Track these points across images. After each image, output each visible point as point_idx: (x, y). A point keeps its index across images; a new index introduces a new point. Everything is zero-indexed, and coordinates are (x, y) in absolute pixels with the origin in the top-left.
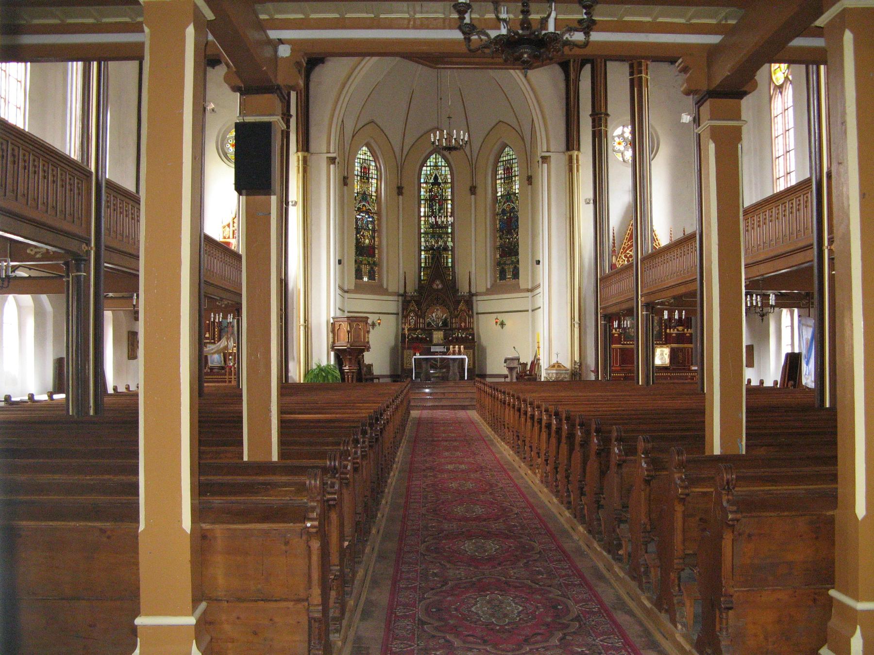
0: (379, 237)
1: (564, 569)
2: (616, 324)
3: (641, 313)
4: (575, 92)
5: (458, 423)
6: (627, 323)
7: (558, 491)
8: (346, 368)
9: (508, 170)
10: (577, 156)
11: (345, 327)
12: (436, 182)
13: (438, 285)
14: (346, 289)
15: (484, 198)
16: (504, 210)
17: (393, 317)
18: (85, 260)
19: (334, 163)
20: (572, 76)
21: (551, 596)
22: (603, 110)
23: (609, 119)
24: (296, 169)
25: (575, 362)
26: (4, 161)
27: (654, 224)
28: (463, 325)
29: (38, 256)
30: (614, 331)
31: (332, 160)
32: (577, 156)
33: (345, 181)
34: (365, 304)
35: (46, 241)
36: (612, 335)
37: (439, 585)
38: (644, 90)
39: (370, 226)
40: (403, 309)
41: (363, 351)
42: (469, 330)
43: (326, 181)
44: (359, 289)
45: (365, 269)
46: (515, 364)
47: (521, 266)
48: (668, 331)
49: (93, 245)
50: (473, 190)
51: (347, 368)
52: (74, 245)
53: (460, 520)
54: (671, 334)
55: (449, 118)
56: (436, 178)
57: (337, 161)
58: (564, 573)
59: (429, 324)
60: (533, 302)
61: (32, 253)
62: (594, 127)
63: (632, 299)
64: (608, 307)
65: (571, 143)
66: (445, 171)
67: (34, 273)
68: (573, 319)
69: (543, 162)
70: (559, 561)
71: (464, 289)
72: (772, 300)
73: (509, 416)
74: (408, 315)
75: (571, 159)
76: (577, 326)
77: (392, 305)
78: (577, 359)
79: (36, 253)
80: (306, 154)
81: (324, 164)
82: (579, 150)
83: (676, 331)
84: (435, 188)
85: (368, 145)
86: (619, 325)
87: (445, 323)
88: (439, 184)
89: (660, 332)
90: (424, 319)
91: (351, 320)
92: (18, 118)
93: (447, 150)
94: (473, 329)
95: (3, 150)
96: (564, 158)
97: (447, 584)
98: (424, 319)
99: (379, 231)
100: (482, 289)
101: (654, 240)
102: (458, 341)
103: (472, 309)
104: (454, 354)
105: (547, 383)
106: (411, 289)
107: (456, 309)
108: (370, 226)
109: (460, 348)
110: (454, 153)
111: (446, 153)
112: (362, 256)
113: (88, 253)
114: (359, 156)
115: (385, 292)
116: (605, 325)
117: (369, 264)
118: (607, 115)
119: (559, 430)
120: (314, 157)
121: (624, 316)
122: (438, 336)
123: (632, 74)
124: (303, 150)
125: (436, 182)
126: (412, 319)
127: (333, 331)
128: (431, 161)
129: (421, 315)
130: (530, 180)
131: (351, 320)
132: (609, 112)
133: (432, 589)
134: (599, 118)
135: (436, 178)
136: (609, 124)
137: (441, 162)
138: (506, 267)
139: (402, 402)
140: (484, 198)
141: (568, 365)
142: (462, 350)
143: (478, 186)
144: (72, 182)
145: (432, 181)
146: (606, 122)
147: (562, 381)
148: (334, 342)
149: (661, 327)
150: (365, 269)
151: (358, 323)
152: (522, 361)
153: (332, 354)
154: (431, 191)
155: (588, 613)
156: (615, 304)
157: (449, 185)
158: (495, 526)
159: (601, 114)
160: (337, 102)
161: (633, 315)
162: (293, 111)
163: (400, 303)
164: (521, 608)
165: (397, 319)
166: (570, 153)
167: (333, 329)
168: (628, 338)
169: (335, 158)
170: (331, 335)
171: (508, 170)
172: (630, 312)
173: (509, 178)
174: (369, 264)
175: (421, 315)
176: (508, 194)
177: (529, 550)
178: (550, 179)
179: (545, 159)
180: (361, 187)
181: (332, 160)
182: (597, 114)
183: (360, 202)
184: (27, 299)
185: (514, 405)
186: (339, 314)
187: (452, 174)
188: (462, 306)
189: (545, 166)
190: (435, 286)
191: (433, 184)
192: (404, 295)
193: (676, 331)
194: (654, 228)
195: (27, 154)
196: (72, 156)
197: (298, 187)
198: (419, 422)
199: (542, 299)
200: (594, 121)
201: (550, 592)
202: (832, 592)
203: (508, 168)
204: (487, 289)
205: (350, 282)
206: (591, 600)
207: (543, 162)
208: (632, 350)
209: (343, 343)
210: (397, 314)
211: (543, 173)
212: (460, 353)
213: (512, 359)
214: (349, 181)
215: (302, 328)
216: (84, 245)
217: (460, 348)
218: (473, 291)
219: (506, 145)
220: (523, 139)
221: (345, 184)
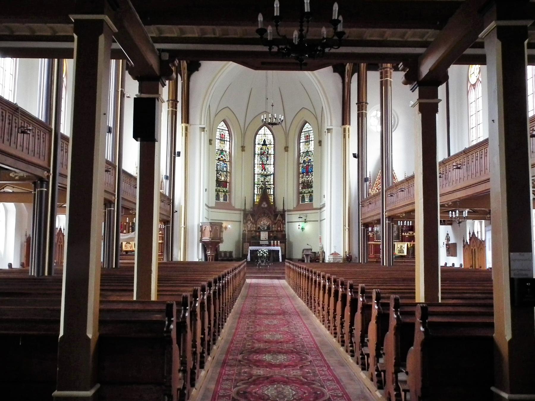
0: (230, 177)
1: (323, 370)
2: (370, 229)
3: (386, 222)
4: (348, 89)
5: (274, 287)
6: (377, 228)
7: (329, 327)
8: (209, 253)
9: (307, 137)
10: (349, 129)
11: (208, 228)
12: (264, 144)
13: (264, 205)
14: (210, 206)
15: (292, 154)
16: (304, 161)
17: (238, 223)
18: (47, 181)
19: (204, 131)
20: (347, 80)
21: (314, 386)
22: (364, 100)
23: (368, 106)
24: (181, 134)
25: (346, 252)
26: (4, 122)
27: (393, 166)
28: (279, 229)
29: (17, 178)
30: (370, 234)
31: (203, 129)
32: (349, 129)
33: (210, 142)
34: (219, 215)
35: (15, 167)
36: (368, 237)
37: (247, 378)
38: (389, 88)
39: (225, 169)
40: (244, 219)
41: (219, 243)
42: (282, 231)
43: (199, 141)
44: (218, 206)
45: (222, 195)
46: (309, 253)
47: (314, 195)
48: (403, 234)
49: (51, 172)
50: (286, 149)
51: (209, 253)
52: (38, 172)
53: (266, 342)
54: (405, 236)
55: (273, 106)
56: (264, 141)
57: (205, 130)
58: (323, 373)
59: (259, 228)
60: (320, 216)
61: (13, 176)
62: (358, 110)
63: (379, 214)
64: (366, 218)
65: (345, 120)
66: (270, 137)
67: (16, 190)
68: (344, 226)
69: (328, 132)
70: (321, 366)
71: (280, 207)
72: (465, 214)
73: (304, 283)
74: (247, 222)
75: (345, 130)
76: (347, 230)
77: (238, 216)
78: (347, 249)
79: (16, 176)
80: (187, 125)
81: (198, 131)
82: (350, 124)
83: (408, 234)
84: (264, 147)
85: (224, 121)
86: (372, 229)
87: (268, 228)
88: (266, 145)
89: (398, 234)
90: (256, 225)
91: (212, 224)
92: (9, 97)
93: (270, 125)
94: (285, 231)
95: (3, 116)
96: (341, 130)
97: (251, 378)
98: (256, 225)
99: (230, 173)
100: (291, 208)
101: (393, 177)
102: (275, 238)
103: (284, 219)
104: (274, 246)
105: (330, 264)
106: (249, 207)
107: (275, 219)
108: (225, 169)
109: (277, 242)
110: (274, 126)
111: (270, 126)
112: (220, 187)
113: (48, 177)
114: (218, 127)
115: (234, 209)
116: (364, 229)
117: (224, 192)
118: (366, 103)
119: (336, 292)
120: (192, 126)
121: (376, 224)
122: (264, 235)
123: (381, 78)
124: (185, 122)
125: (264, 144)
126: (249, 225)
127: (201, 231)
128: (262, 131)
129: (255, 223)
130: (320, 142)
131: (212, 224)
132: (368, 102)
133: (242, 380)
134: (362, 105)
135: (264, 141)
136: (367, 109)
137: (268, 132)
138: (305, 195)
139: (239, 272)
140: (292, 154)
141: (342, 254)
142: (279, 243)
143: (289, 147)
144: (39, 134)
145: (262, 143)
146: (366, 108)
147: (338, 263)
148: (202, 238)
149: (399, 232)
150: (222, 195)
151: (217, 228)
152: (313, 251)
153: (201, 244)
154: (261, 149)
155: (336, 396)
156: (370, 217)
157: (273, 146)
158: (285, 346)
159: (363, 103)
160: (206, 95)
161: (380, 224)
162: (179, 99)
163: (242, 214)
164: (294, 393)
165: (240, 225)
166: (344, 126)
167: (202, 230)
168: (378, 238)
169: (204, 128)
170: (200, 233)
171: (307, 137)
172: (378, 222)
173: (307, 141)
174: (224, 192)
175: (255, 223)
176: (307, 152)
177: (304, 359)
178: (332, 143)
179: (329, 130)
180: (220, 146)
181: (203, 129)
182: (361, 103)
183: (220, 155)
184: (11, 206)
185: (306, 275)
186: (205, 221)
187: (274, 140)
188: (279, 217)
189: (329, 134)
190: (263, 206)
191: (263, 145)
192: (244, 210)
193: (408, 234)
194: (394, 169)
195: (4, 112)
196: (40, 119)
197: (182, 145)
198: (250, 286)
199: (326, 213)
200: (358, 107)
201: (314, 384)
202: (493, 389)
203: (307, 136)
204: (294, 208)
205: (213, 203)
206: (338, 389)
207: (328, 132)
208: (379, 245)
209: (207, 238)
210: (240, 222)
211: (327, 139)
212: (277, 245)
213: (307, 250)
214: (212, 142)
215: (183, 229)
216: (46, 172)
217: (277, 242)
218: (286, 209)
219: (306, 122)
220: (316, 118)
221: (210, 144)
